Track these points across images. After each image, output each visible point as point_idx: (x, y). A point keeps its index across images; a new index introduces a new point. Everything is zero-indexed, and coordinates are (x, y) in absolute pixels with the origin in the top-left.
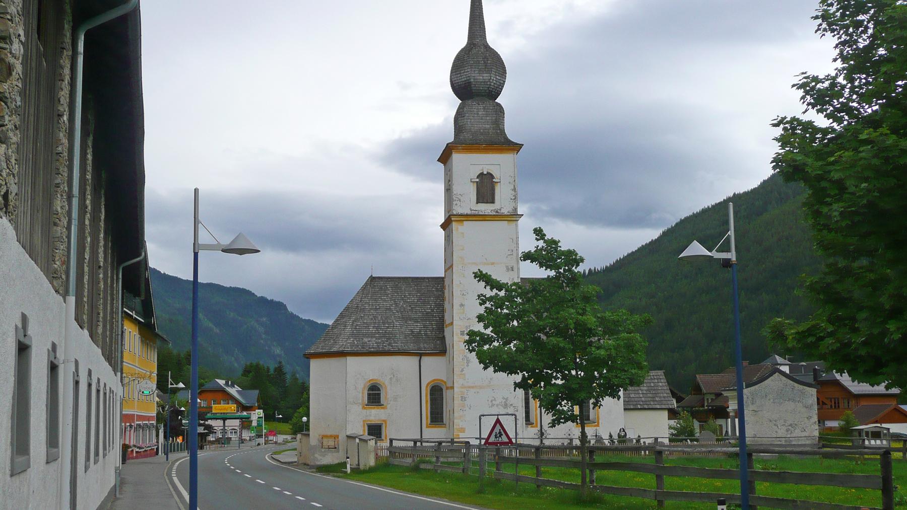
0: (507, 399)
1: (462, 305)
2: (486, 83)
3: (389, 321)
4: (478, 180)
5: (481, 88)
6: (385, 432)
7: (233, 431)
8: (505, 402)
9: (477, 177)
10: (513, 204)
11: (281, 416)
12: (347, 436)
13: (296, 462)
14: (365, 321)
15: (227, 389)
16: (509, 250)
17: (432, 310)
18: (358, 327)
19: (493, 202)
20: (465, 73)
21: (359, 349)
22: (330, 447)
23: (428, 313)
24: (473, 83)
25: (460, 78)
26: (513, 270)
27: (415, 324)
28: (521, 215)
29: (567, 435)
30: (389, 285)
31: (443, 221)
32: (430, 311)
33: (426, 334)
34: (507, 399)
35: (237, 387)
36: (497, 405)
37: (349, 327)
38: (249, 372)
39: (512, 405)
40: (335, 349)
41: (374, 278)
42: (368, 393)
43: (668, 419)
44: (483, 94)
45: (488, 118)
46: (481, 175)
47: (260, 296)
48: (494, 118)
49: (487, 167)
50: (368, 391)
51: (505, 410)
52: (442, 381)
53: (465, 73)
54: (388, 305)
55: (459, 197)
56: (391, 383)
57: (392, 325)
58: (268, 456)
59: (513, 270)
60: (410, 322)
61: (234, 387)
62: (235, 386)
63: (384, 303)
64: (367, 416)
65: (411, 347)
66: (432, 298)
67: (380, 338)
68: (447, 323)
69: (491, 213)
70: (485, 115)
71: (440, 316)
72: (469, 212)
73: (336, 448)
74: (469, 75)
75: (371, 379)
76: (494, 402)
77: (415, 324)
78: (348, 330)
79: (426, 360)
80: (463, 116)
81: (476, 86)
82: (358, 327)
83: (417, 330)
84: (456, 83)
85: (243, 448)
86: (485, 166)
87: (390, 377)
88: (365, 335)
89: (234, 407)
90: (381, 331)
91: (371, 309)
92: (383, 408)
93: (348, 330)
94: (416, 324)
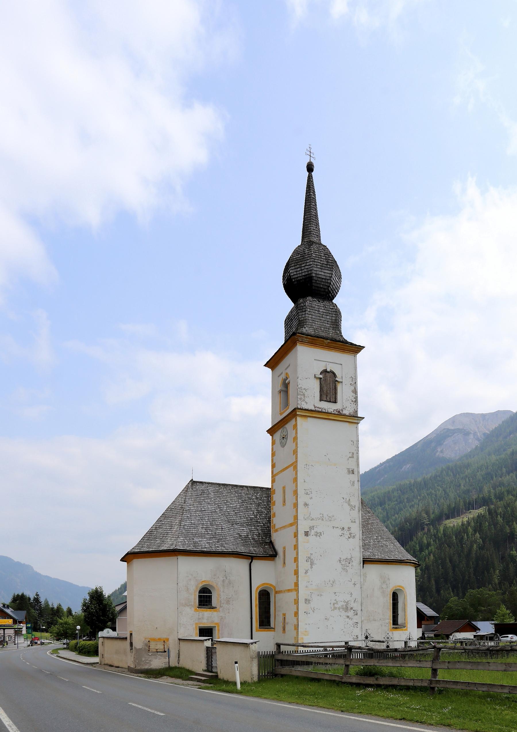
0: (347, 603)
1: (306, 505)
2: (326, 281)
3: (217, 523)
4: (321, 376)
5: (321, 286)
6: (218, 635)
7: (9, 637)
8: (346, 606)
9: (321, 374)
10: (353, 405)
11: (44, 627)
12: (179, 639)
13: (98, 663)
14: (193, 522)
15: (4, 609)
16: (350, 453)
17: (256, 517)
18: (186, 527)
19: (335, 402)
20: (307, 267)
21: (191, 548)
22: (158, 651)
23: (251, 519)
24: (315, 278)
25: (300, 272)
26: (353, 473)
27: (241, 528)
28: (360, 417)
29: (386, 638)
30: (211, 489)
31: (271, 427)
32: (253, 517)
33: (253, 539)
34: (347, 603)
35: (11, 609)
36: (339, 609)
37: (176, 527)
38: (16, 600)
39: (352, 608)
40: (164, 547)
41: (194, 482)
42: (199, 595)
43: (417, 628)
44: (322, 293)
45: (328, 317)
46: (325, 372)
47: (17, 561)
48: (334, 318)
49: (331, 364)
50: (199, 593)
51: (346, 613)
52: (271, 585)
53: (307, 267)
54: (213, 508)
55: (304, 391)
56: (224, 586)
57: (220, 528)
58: (49, 653)
59: (353, 473)
60: (236, 526)
61: (9, 609)
62: (10, 608)
63: (209, 506)
64: (199, 619)
65: (241, 549)
66: (253, 506)
67: (210, 539)
68: (277, 527)
69: (333, 412)
70: (325, 314)
71: (264, 523)
72: (313, 409)
73: (165, 652)
74: (311, 269)
75: (203, 580)
76: (336, 606)
77: (241, 528)
78: (175, 529)
79: (257, 564)
80: (304, 310)
81: (317, 282)
82: (186, 527)
83: (244, 534)
84: (294, 278)
85: (20, 648)
86: (328, 363)
87: (222, 579)
88: (195, 535)
89: (11, 621)
90: (210, 533)
91: (197, 510)
92: (216, 611)
93: (175, 529)
94: (243, 529)
